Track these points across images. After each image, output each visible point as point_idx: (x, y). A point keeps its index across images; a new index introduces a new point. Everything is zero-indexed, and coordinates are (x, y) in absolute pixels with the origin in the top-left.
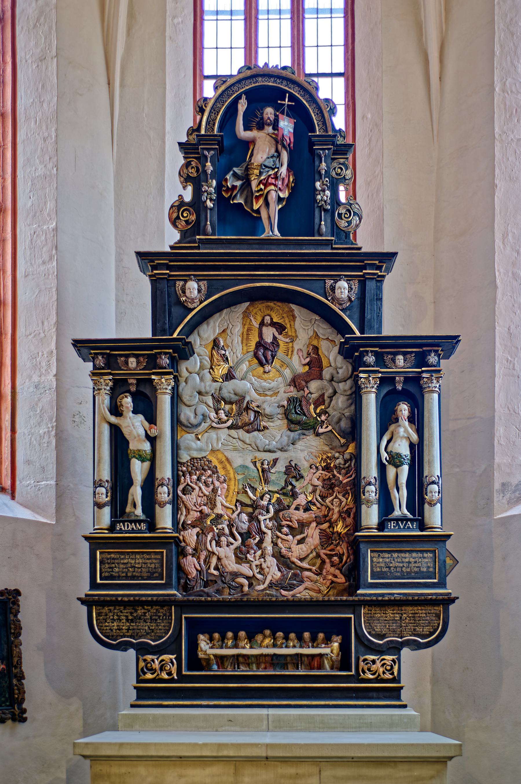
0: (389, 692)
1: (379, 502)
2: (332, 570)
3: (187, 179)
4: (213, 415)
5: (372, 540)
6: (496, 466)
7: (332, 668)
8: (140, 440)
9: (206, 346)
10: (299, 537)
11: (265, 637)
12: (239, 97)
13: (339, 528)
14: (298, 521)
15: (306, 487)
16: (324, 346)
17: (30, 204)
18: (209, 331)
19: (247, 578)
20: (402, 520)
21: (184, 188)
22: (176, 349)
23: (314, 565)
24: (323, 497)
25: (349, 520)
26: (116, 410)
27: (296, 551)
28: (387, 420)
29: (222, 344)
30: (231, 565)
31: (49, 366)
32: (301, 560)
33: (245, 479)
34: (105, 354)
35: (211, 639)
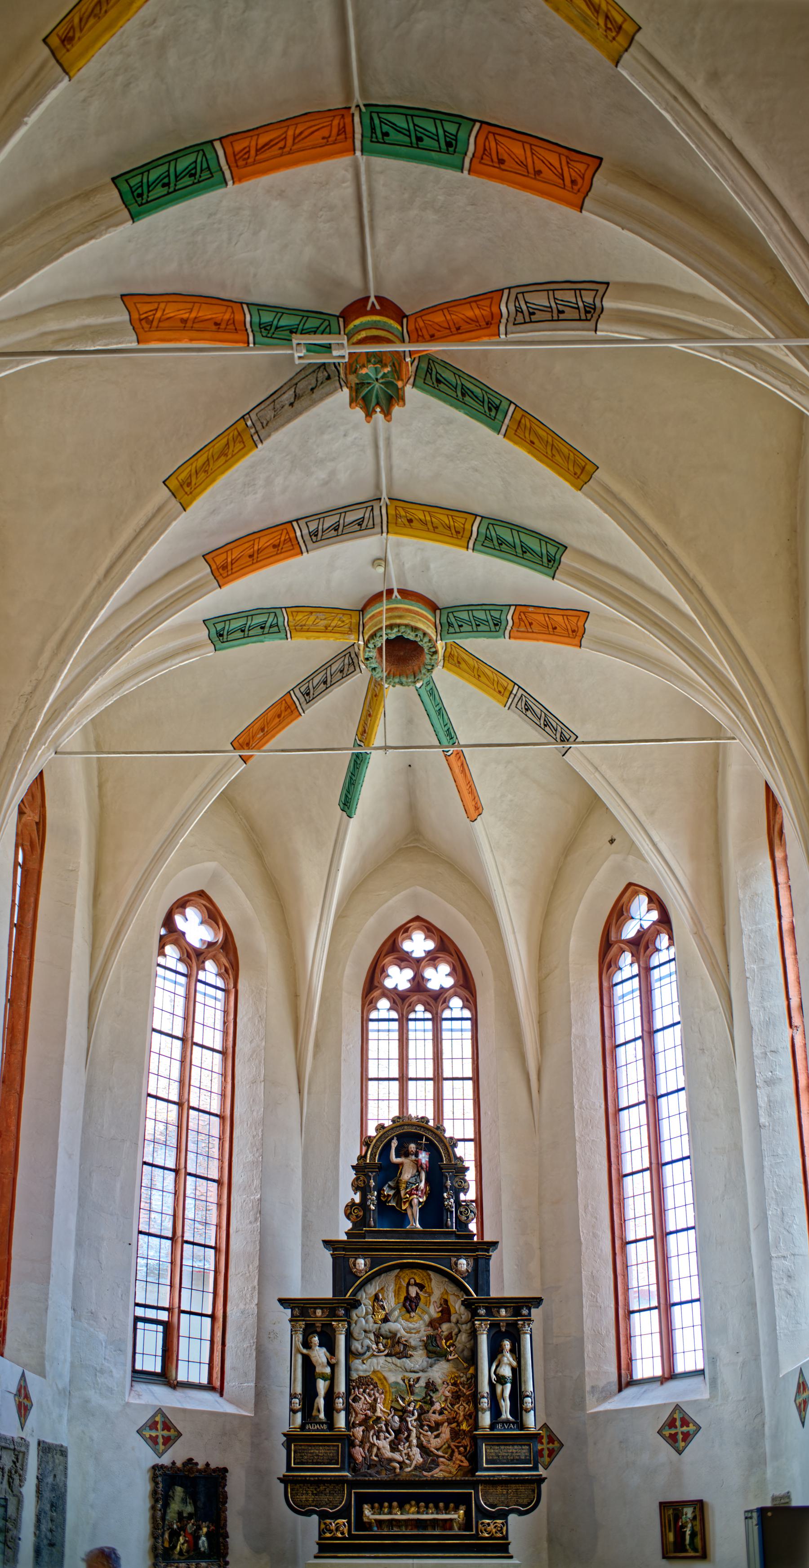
0: (501, 1548)
1: (491, 1409)
2: (460, 1457)
3: (356, 1188)
4: (374, 1346)
5: (487, 1438)
6: (586, 1373)
7: (459, 1529)
8: (323, 1366)
9: (369, 1299)
10: (435, 1433)
11: (411, 1506)
12: (392, 1139)
13: (464, 1426)
14: (435, 1422)
15: (440, 1397)
16: (451, 1299)
17: (241, 1180)
18: (372, 1289)
19: (399, 1463)
20: (506, 1423)
21: (355, 1194)
22: (348, 1304)
23: (446, 1453)
24: (452, 1405)
25: (471, 1421)
26: (307, 1344)
27: (434, 1443)
28: (495, 1353)
29: (381, 1297)
30: (388, 1453)
31: (252, 1297)
32: (438, 1450)
33: (397, 1392)
34: (299, 1308)
35: (373, 1508)
